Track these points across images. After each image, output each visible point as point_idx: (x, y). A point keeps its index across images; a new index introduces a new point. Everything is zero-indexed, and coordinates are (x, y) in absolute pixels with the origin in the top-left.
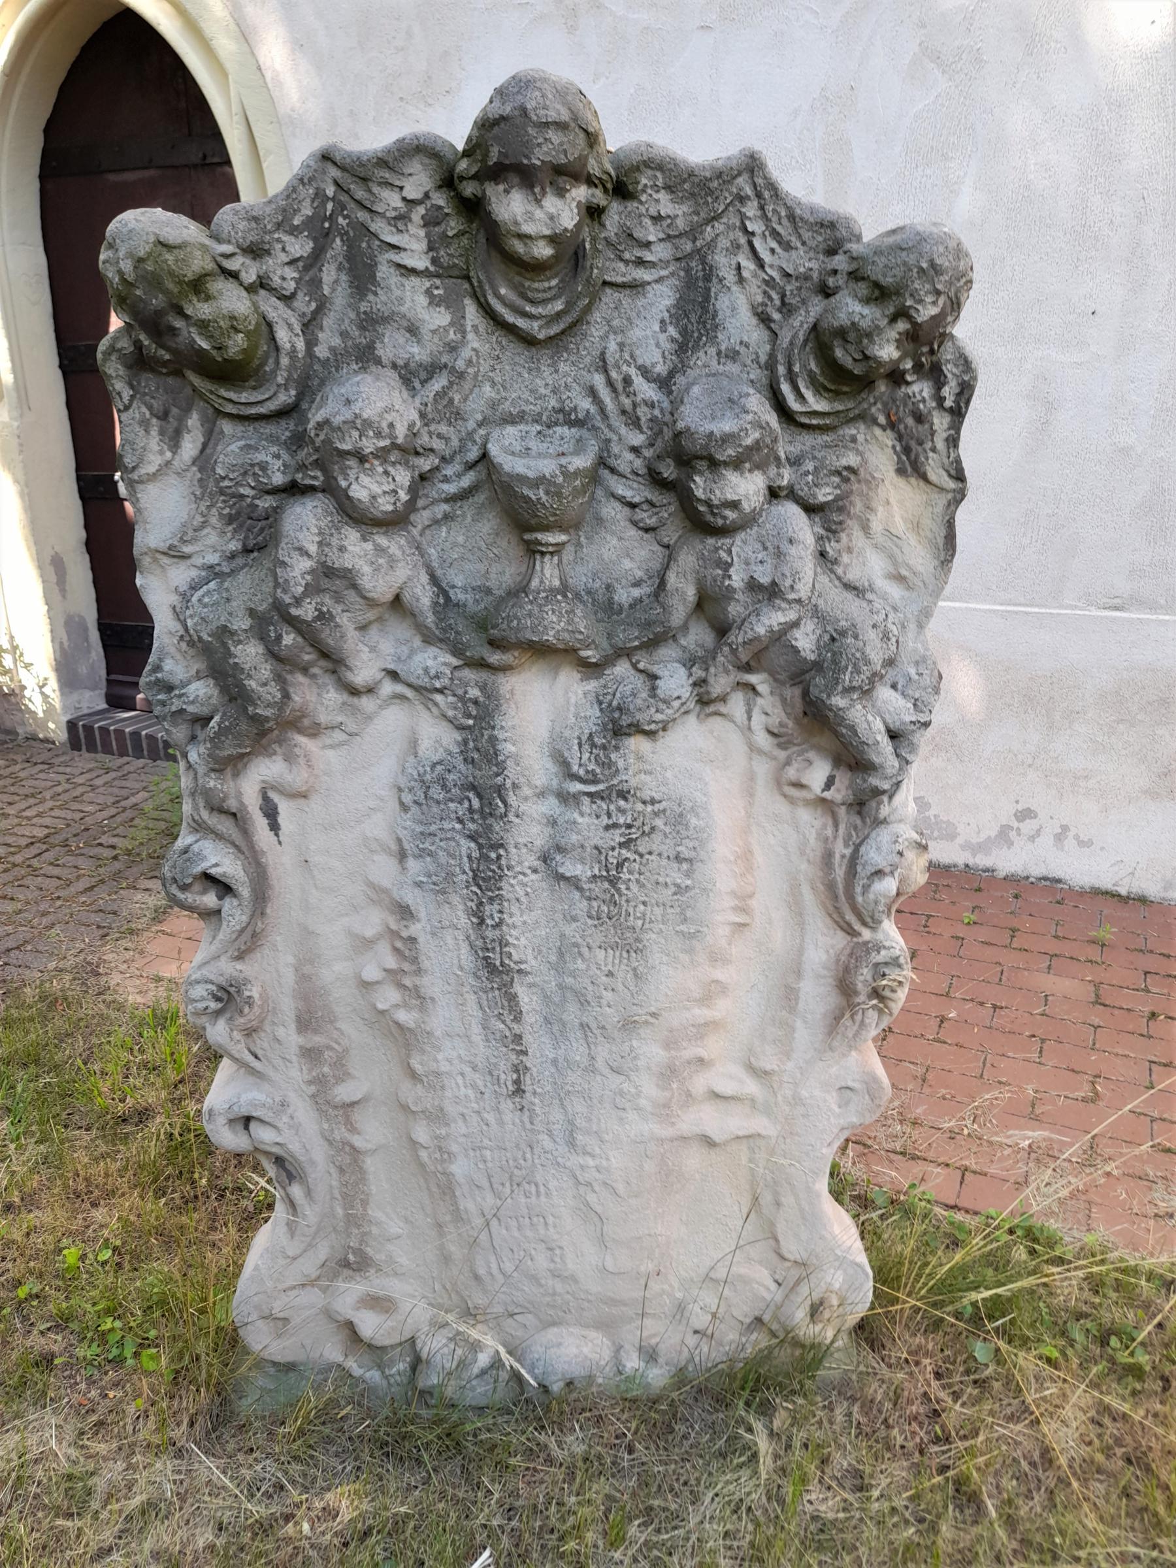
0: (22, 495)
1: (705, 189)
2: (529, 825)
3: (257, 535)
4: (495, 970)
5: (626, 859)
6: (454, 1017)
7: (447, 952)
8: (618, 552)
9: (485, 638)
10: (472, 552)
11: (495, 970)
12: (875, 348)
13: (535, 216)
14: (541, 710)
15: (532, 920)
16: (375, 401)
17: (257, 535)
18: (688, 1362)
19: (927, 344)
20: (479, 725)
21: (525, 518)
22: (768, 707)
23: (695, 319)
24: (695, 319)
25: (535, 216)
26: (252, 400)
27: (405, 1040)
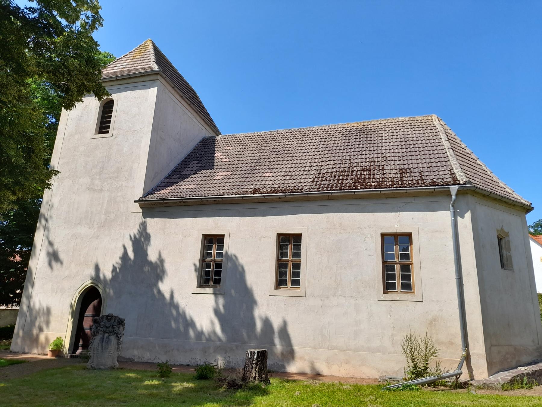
0: (198, 277)
1: (115, 317)
2: (105, 340)
3: (97, 328)
4: (102, 346)
5: (109, 341)
6: (100, 348)
7: (100, 345)
8: (111, 329)
9: (105, 332)
10: (105, 329)
11: (102, 346)
12: (121, 322)
13: (109, 318)
14: (106, 335)
15: (104, 344)
16: (103, 323)
17: (97, 328)
18: (25, 71)
19: (122, 322)
20: (104, 336)
21: (107, 327)
22: (115, 335)
23: (115, 321)
24: (115, 321)
25: (109, 318)
26: (394, 299)
27: (97, 350)
